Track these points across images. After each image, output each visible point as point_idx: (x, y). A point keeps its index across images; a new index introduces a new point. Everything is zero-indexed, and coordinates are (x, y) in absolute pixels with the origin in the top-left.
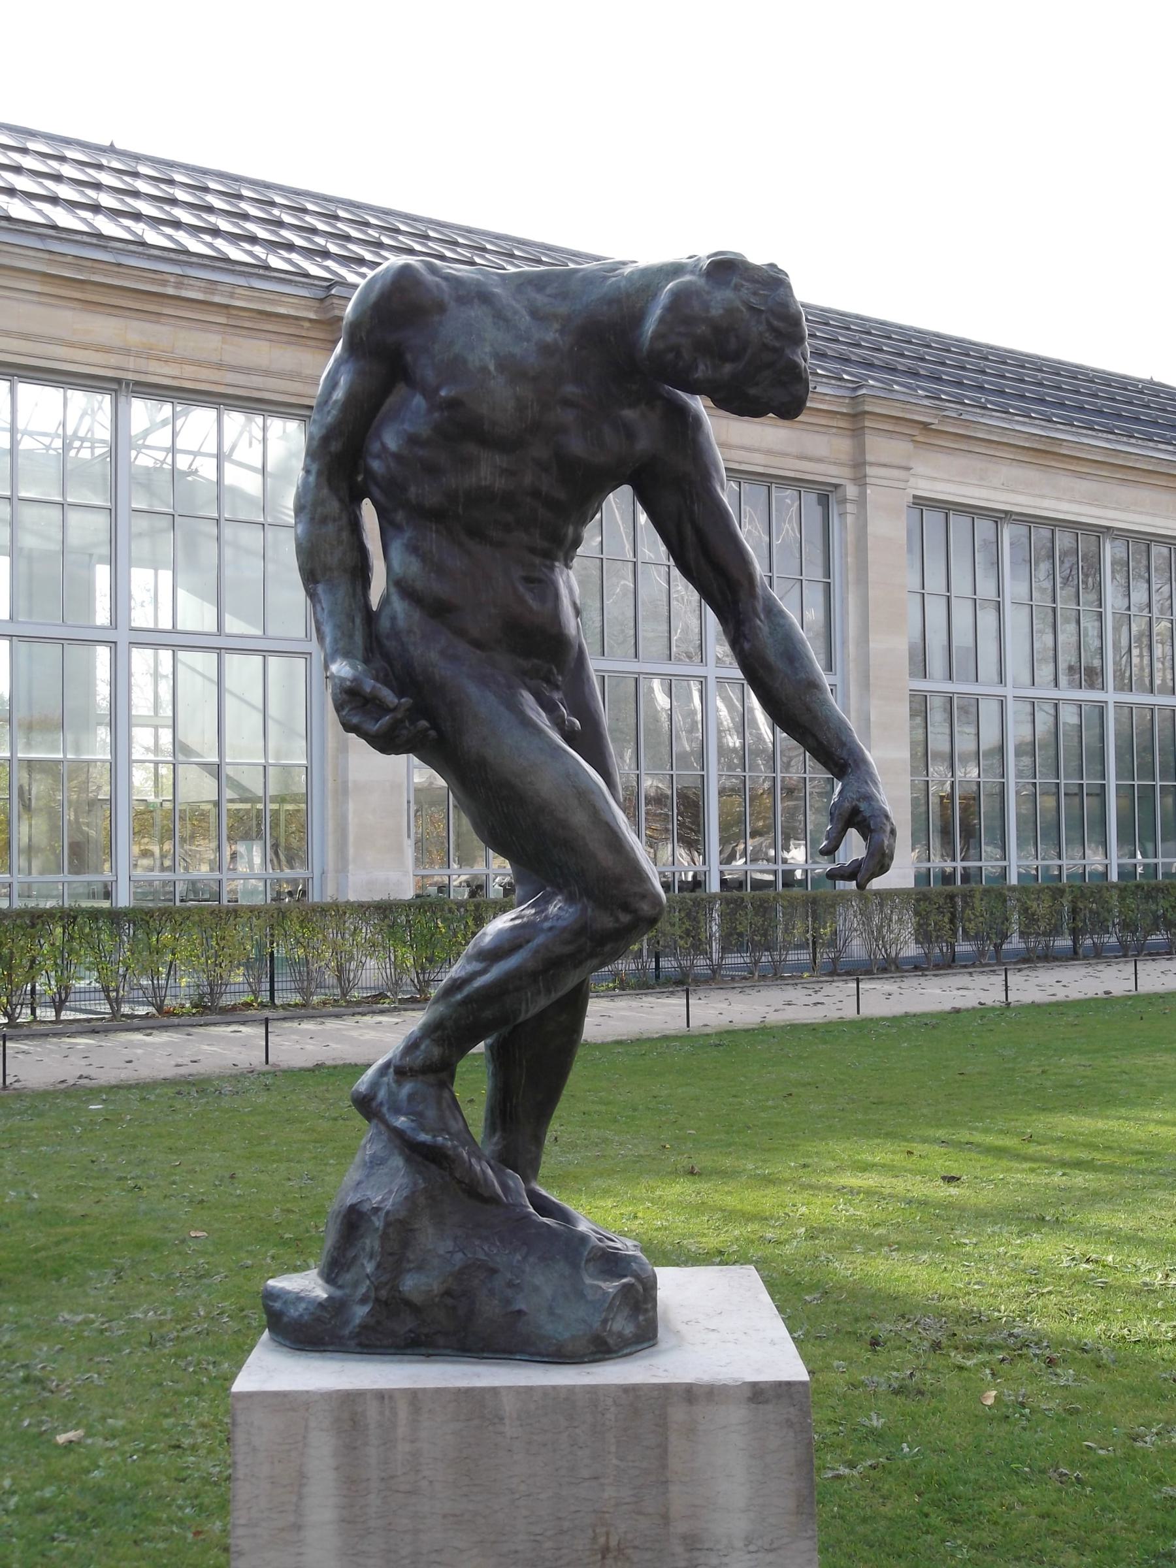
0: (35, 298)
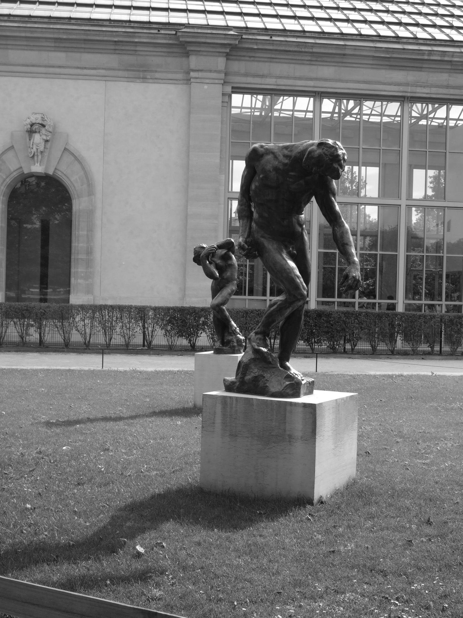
0: (370, 66)
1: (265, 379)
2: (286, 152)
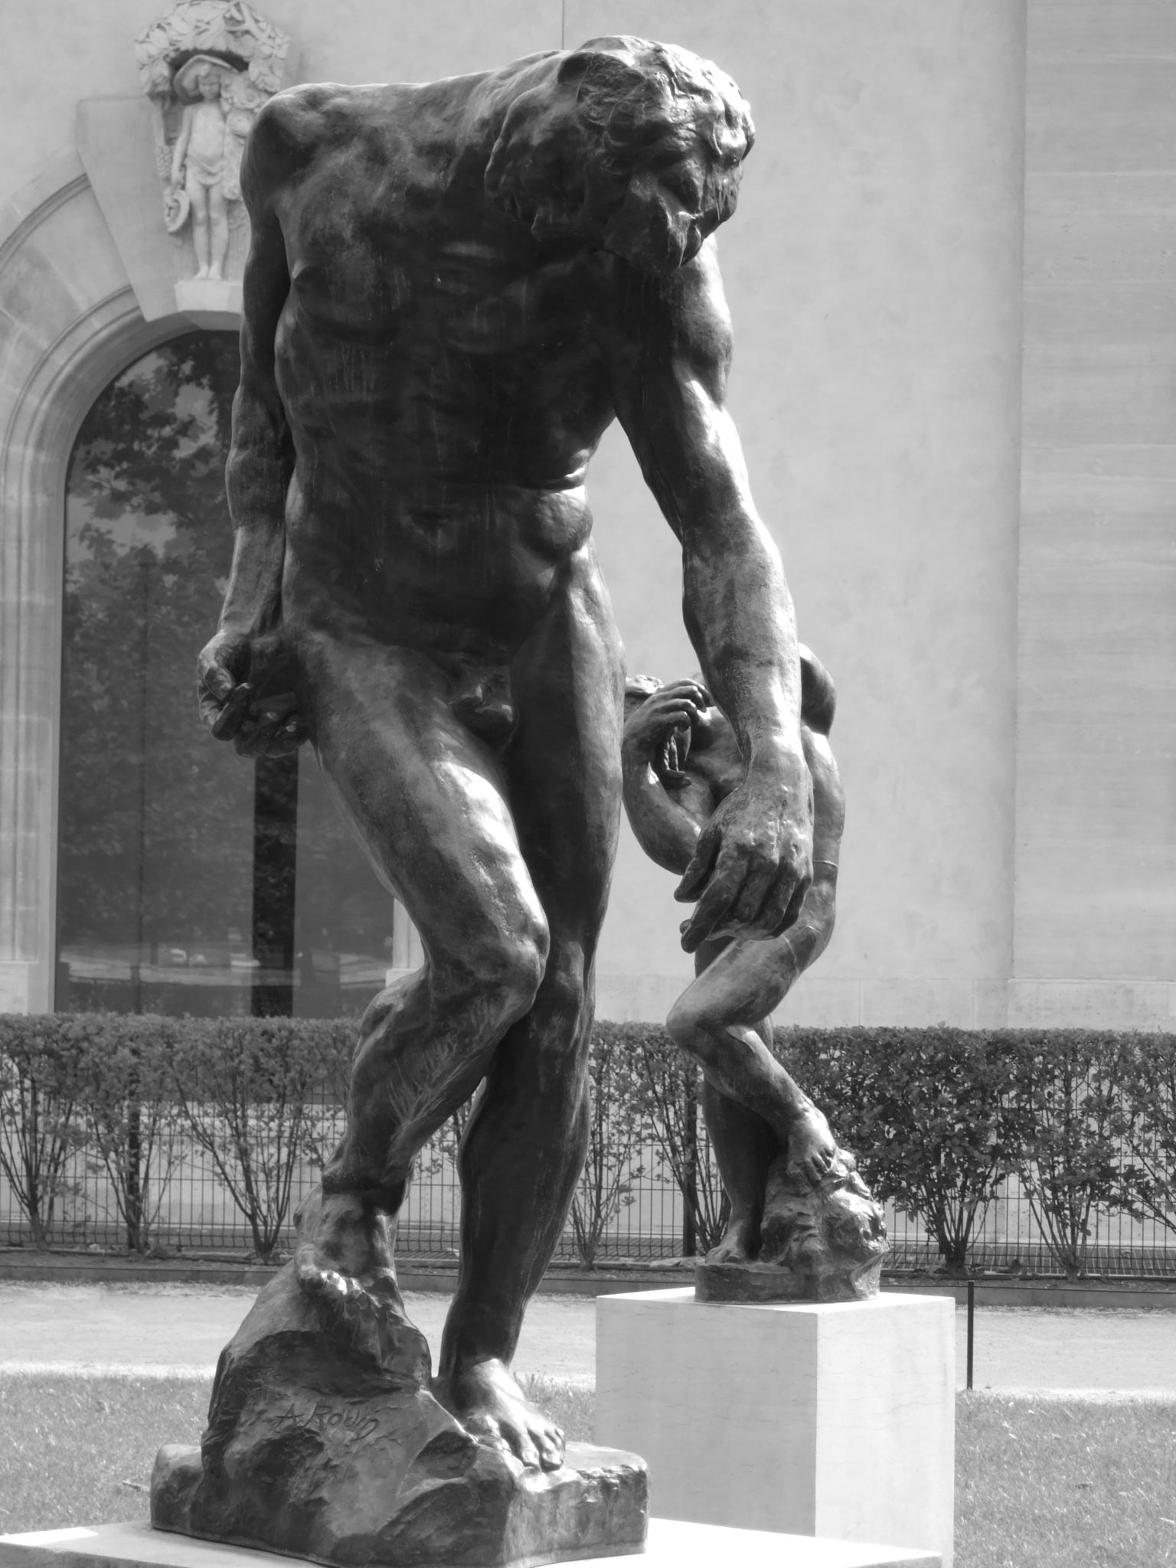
1: (321, 1459)
2: (433, 126)
